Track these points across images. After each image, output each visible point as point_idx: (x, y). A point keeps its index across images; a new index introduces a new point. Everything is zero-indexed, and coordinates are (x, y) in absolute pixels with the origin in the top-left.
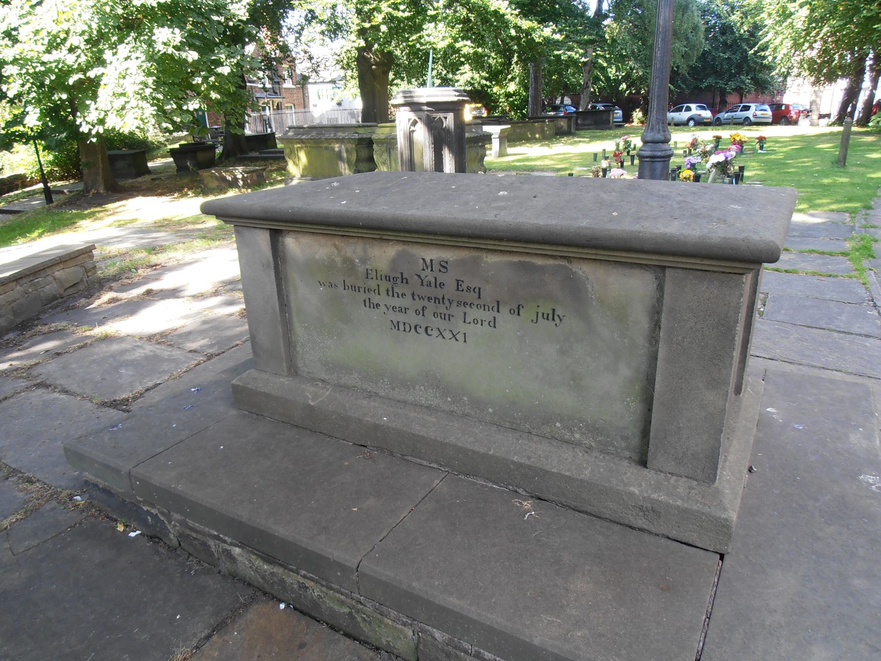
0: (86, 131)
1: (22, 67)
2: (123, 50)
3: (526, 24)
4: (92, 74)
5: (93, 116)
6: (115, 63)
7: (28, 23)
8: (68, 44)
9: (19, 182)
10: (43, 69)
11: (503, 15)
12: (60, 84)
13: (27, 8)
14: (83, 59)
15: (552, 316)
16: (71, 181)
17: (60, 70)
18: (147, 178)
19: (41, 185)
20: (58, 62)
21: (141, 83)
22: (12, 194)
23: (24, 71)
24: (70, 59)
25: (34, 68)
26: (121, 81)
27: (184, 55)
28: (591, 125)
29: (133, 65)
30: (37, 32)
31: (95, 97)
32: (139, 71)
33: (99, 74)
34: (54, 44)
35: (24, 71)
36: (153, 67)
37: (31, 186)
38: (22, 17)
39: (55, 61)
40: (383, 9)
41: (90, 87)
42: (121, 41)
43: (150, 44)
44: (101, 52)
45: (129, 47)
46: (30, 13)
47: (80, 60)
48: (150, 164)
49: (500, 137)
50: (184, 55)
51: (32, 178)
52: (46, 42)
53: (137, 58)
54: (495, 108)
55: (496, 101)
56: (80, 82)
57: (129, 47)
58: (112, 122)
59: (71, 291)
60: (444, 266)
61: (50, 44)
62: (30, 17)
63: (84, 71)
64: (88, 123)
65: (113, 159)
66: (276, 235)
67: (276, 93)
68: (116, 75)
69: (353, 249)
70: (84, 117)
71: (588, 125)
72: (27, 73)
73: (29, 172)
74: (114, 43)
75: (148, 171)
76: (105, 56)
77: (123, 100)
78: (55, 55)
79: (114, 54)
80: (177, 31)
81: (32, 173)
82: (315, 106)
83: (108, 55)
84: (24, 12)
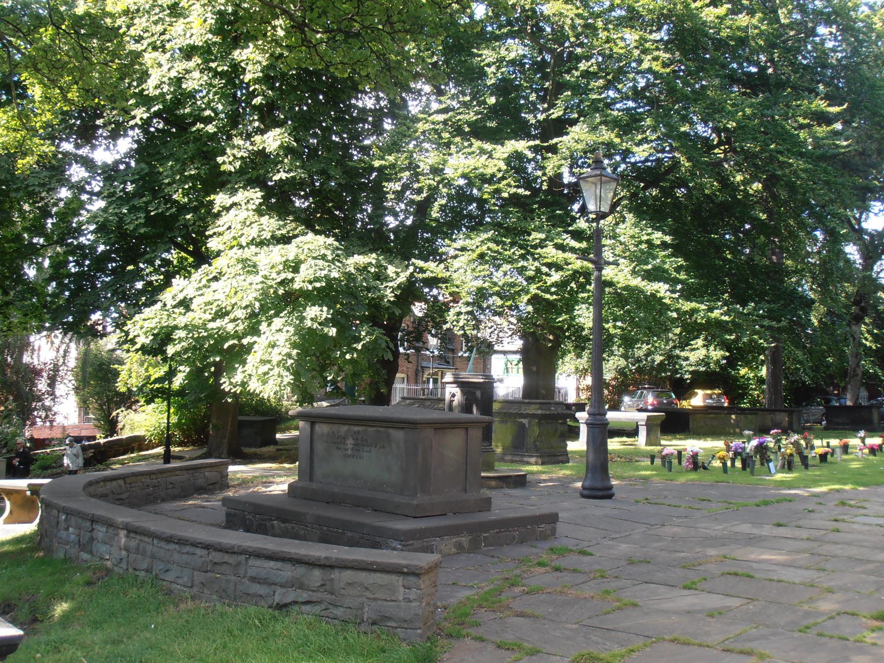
0: (227, 390)
1: (190, 331)
2: (278, 322)
3: (687, 306)
4: (245, 341)
5: (238, 377)
6: (268, 334)
7: (202, 295)
8: (232, 316)
9: (136, 445)
10: (206, 334)
11: (661, 298)
12: (216, 349)
13: (204, 282)
14: (241, 327)
15: (383, 447)
16: (190, 448)
17: (219, 336)
18: (271, 449)
19: (160, 450)
20: (219, 329)
21: (286, 355)
22: (125, 457)
23: (191, 335)
24: (230, 327)
25: (199, 333)
26: (270, 350)
27: (326, 330)
28: (847, 424)
29: (282, 338)
30: (206, 304)
31: (244, 363)
32: (287, 343)
33: (252, 341)
34: (221, 314)
35: (191, 335)
36: (302, 337)
37: (147, 450)
38: (200, 289)
39: (218, 328)
40: (531, 290)
41: (240, 353)
42: (277, 315)
43: (302, 319)
44: (259, 323)
45: (284, 320)
46: (205, 286)
47: (237, 328)
48: (278, 436)
49: (646, 425)
50: (326, 330)
51: (151, 441)
52: (213, 312)
53: (288, 331)
54: (742, 397)
55: (745, 388)
56: (232, 347)
57: (284, 320)
58: (254, 386)
59: (210, 487)
60: (359, 432)
61: (216, 313)
62: (204, 290)
63: (240, 338)
64: (231, 383)
65: (242, 425)
66: (313, 424)
67: (448, 363)
68: (267, 343)
69: (335, 428)
70: (230, 378)
71: (843, 424)
72: (192, 338)
73: (149, 434)
74: (271, 316)
75: (275, 442)
76: (261, 328)
77: (268, 366)
78: (218, 323)
79: (269, 325)
80: (325, 309)
81: (151, 436)
82: (501, 381)
83: (263, 327)
84: (201, 285)
